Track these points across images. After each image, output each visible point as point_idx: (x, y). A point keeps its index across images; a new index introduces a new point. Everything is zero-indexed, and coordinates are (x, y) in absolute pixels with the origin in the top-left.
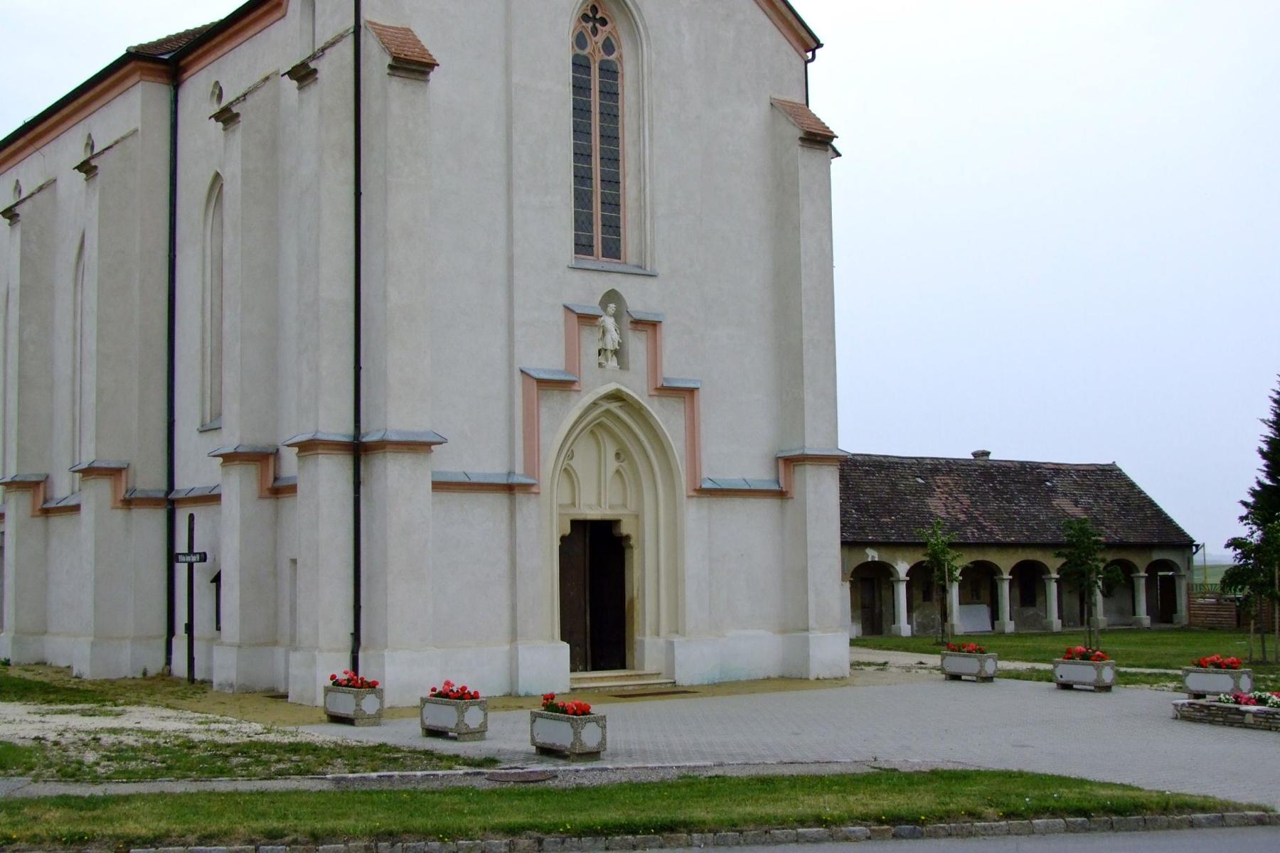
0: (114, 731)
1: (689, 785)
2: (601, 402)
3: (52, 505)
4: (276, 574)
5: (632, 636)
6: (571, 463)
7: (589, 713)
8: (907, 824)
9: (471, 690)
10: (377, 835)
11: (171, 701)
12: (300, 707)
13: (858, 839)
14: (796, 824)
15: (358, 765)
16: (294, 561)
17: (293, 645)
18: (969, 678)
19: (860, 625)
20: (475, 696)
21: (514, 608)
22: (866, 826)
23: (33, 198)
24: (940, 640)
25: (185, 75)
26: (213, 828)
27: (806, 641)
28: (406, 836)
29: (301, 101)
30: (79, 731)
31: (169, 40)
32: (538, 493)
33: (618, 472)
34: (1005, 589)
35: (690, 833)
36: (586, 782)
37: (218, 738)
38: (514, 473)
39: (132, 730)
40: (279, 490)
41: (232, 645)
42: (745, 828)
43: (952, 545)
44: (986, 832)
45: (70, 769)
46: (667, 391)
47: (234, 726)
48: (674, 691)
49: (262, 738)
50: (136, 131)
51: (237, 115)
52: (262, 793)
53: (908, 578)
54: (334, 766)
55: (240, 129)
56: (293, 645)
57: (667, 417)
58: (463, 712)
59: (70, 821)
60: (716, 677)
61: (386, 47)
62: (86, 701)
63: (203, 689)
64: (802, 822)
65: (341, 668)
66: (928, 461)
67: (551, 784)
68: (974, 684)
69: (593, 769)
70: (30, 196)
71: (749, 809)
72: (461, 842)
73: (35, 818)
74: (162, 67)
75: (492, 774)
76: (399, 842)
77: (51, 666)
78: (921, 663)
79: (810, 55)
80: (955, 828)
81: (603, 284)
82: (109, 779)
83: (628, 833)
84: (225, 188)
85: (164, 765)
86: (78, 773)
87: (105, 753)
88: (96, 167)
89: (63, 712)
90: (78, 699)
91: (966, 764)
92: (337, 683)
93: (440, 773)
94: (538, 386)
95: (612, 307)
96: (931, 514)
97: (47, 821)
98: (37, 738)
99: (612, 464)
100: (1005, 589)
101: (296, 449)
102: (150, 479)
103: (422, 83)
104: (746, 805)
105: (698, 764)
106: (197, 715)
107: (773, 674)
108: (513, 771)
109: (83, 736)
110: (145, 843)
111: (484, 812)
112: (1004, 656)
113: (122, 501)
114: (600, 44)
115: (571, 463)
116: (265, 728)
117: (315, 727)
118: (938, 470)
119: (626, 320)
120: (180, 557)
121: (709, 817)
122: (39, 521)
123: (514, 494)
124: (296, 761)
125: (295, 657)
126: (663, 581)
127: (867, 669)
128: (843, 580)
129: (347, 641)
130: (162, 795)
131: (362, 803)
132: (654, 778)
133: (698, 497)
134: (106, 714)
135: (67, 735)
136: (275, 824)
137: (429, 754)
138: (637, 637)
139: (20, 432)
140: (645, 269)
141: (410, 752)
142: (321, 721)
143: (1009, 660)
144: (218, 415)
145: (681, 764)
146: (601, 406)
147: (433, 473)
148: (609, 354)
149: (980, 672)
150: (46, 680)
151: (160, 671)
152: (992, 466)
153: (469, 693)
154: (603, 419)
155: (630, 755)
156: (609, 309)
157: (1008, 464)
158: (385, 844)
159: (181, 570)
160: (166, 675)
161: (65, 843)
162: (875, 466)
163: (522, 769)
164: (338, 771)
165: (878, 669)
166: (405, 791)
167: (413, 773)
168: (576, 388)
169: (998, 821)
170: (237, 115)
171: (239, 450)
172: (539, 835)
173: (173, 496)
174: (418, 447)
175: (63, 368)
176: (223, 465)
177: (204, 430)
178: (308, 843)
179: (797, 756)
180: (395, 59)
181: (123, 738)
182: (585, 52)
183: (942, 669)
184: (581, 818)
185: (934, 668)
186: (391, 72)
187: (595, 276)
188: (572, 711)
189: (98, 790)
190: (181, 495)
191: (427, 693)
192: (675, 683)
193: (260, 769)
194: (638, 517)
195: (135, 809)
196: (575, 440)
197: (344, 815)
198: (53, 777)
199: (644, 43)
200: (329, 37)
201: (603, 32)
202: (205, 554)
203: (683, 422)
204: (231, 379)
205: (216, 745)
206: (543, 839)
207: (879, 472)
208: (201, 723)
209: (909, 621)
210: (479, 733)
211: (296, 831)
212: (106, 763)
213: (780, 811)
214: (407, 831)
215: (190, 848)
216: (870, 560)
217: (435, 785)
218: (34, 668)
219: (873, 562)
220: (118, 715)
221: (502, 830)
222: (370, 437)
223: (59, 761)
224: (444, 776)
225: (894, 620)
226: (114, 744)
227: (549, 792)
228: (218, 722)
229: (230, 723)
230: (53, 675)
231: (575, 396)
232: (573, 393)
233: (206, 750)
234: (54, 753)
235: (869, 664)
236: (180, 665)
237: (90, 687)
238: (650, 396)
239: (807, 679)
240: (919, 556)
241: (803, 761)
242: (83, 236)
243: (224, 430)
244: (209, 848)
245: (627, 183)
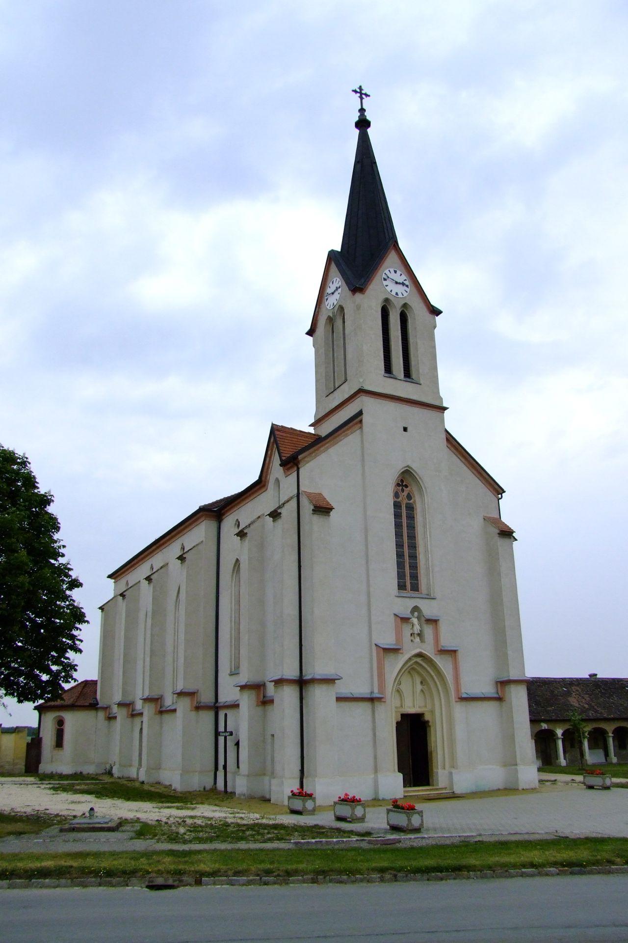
0: (192, 817)
1: (466, 846)
2: (413, 658)
3: (164, 709)
4: (264, 741)
5: (432, 770)
6: (400, 687)
7: (415, 809)
8: (577, 867)
9: (357, 797)
10: (318, 872)
11: (217, 802)
12: (277, 806)
13: (553, 875)
14: (521, 867)
15: (305, 835)
16: (273, 736)
17: (273, 775)
18: (598, 787)
19: (541, 761)
20: (360, 801)
21: (375, 758)
22: (556, 868)
23: (158, 571)
24: (581, 767)
25: (224, 517)
26: (240, 868)
27: (516, 771)
28: (331, 873)
29: (274, 526)
30: (176, 817)
31: (217, 502)
32: (385, 702)
33: (422, 691)
34: (611, 741)
35: (468, 871)
36: (415, 844)
37: (239, 821)
38: (374, 692)
39: (200, 817)
40: (266, 702)
41: (244, 776)
42: (496, 869)
43: (583, 720)
44: (618, 872)
45: (173, 836)
46: (443, 652)
47: (246, 815)
48: (453, 796)
49: (260, 821)
50: (202, 542)
51: (246, 533)
52: (262, 850)
53: (562, 737)
54: (295, 836)
55: (247, 539)
56: (273, 775)
57: (444, 664)
58: (354, 809)
59: (174, 863)
60: (473, 788)
61: (311, 501)
62: (178, 802)
63: (231, 796)
64: (524, 866)
65: (296, 788)
66: (568, 680)
67: (398, 845)
68: (601, 791)
69: (418, 838)
70: (157, 571)
71: (497, 859)
72: (357, 876)
73: (159, 861)
75: (369, 840)
76: (327, 876)
77: (162, 784)
78: (573, 780)
79: (500, 496)
80: (602, 869)
81: (411, 603)
82: (190, 842)
83: (438, 872)
84: (241, 565)
85: (215, 835)
86: (177, 838)
87: (188, 828)
88: (185, 558)
89: (168, 807)
90: (175, 801)
91: (602, 834)
92: (294, 794)
93: (344, 839)
94: (383, 652)
95: (416, 614)
96: (571, 705)
97: (164, 863)
98: (157, 820)
99: (419, 687)
100: (611, 741)
101: (274, 683)
102: (207, 697)
103: (327, 517)
104: (495, 857)
105: (469, 834)
106: (229, 809)
107: (501, 787)
108: (380, 839)
109: (178, 819)
110: (209, 875)
111: (368, 861)
112: (615, 776)
113: (195, 707)
114: (405, 496)
115: (400, 687)
116: (261, 816)
117: (284, 816)
118: (573, 683)
119: (423, 619)
120: (221, 734)
121: (477, 863)
122: (158, 717)
123: (374, 702)
124: (276, 833)
125: (274, 781)
126: (446, 743)
127: (547, 783)
128: (532, 739)
129: (298, 774)
130: (215, 850)
131: (310, 855)
132: (448, 842)
133: (460, 701)
134: (188, 809)
135: (171, 819)
136: (268, 866)
137: (339, 830)
138: (435, 770)
139: (150, 676)
140: (430, 596)
141: (329, 829)
142: (287, 813)
143: (617, 777)
144: (238, 667)
145: (461, 835)
146: (413, 660)
147: (336, 693)
148: (416, 636)
149: (603, 785)
150: (161, 791)
151: (211, 787)
152: (599, 681)
153: (356, 799)
154: (414, 666)
155: (435, 830)
156: (415, 615)
157: (606, 679)
158: (321, 877)
159: (221, 739)
160: (214, 789)
161: (173, 874)
162: (542, 683)
163: (384, 837)
164: (296, 838)
165: (552, 784)
166: (329, 849)
167: (332, 840)
168: (401, 651)
169: (623, 865)
170: (246, 533)
171: (248, 684)
172: (395, 873)
173: (217, 705)
174: (329, 681)
175: (169, 648)
176: (240, 690)
177: (231, 674)
178: (284, 876)
179: (517, 830)
180: (315, 507)
181: (196, 821)
182: (399, 500)
183: (584, 783)
184: (415, 864)
185: (580, 782)
186: (313, 512)
187: (408, 600)
188: (406, 808)
189: (186, 847)
190: (221, 704)
191: (337, 799)
192: (453, 792)
193: (259, 837)
194: (432, 712)
195: (203, 857)
197: (301, 862)
198: (165, 840)
199: (425, 494)
200: (286, 498)
201: (407, 491)
202: (232, 732)
203: (451, 666)
204: (244, 652)
205: (238, 825)
206: (397, 875)
208: (231, 814)
209: (565, 758)
210: (362, 819)
211: (279, 870)
212: (189, 833)
213: (512, 861)
214: (332, 871)
215: (230, 878)
216: (543, 728)
217: (343, 846)
218: (156, 785)
219: (545, 730)
220: (193, 809)
221: (377, 870)
222: (307, 677)
223: (168, 832)
224: (346, 841)
225: (557, 757)
226: (192, 824)
227: (398, 850)
228: (238, 813)
229: (245, 814)
230: (164, 789)
231: (401, 655)
232: (399, 654)
233: (234, 827)
234: (166, 828)
235: (547, 781)
236: (220, 785)
237: (180, 795)
238: (435, 654)
239: (518, 789)
240: (567, 726)
241: (521, 832)
242: (179, 587)
243: (241, 675)
244: (238, 878)
245: (420, 557)
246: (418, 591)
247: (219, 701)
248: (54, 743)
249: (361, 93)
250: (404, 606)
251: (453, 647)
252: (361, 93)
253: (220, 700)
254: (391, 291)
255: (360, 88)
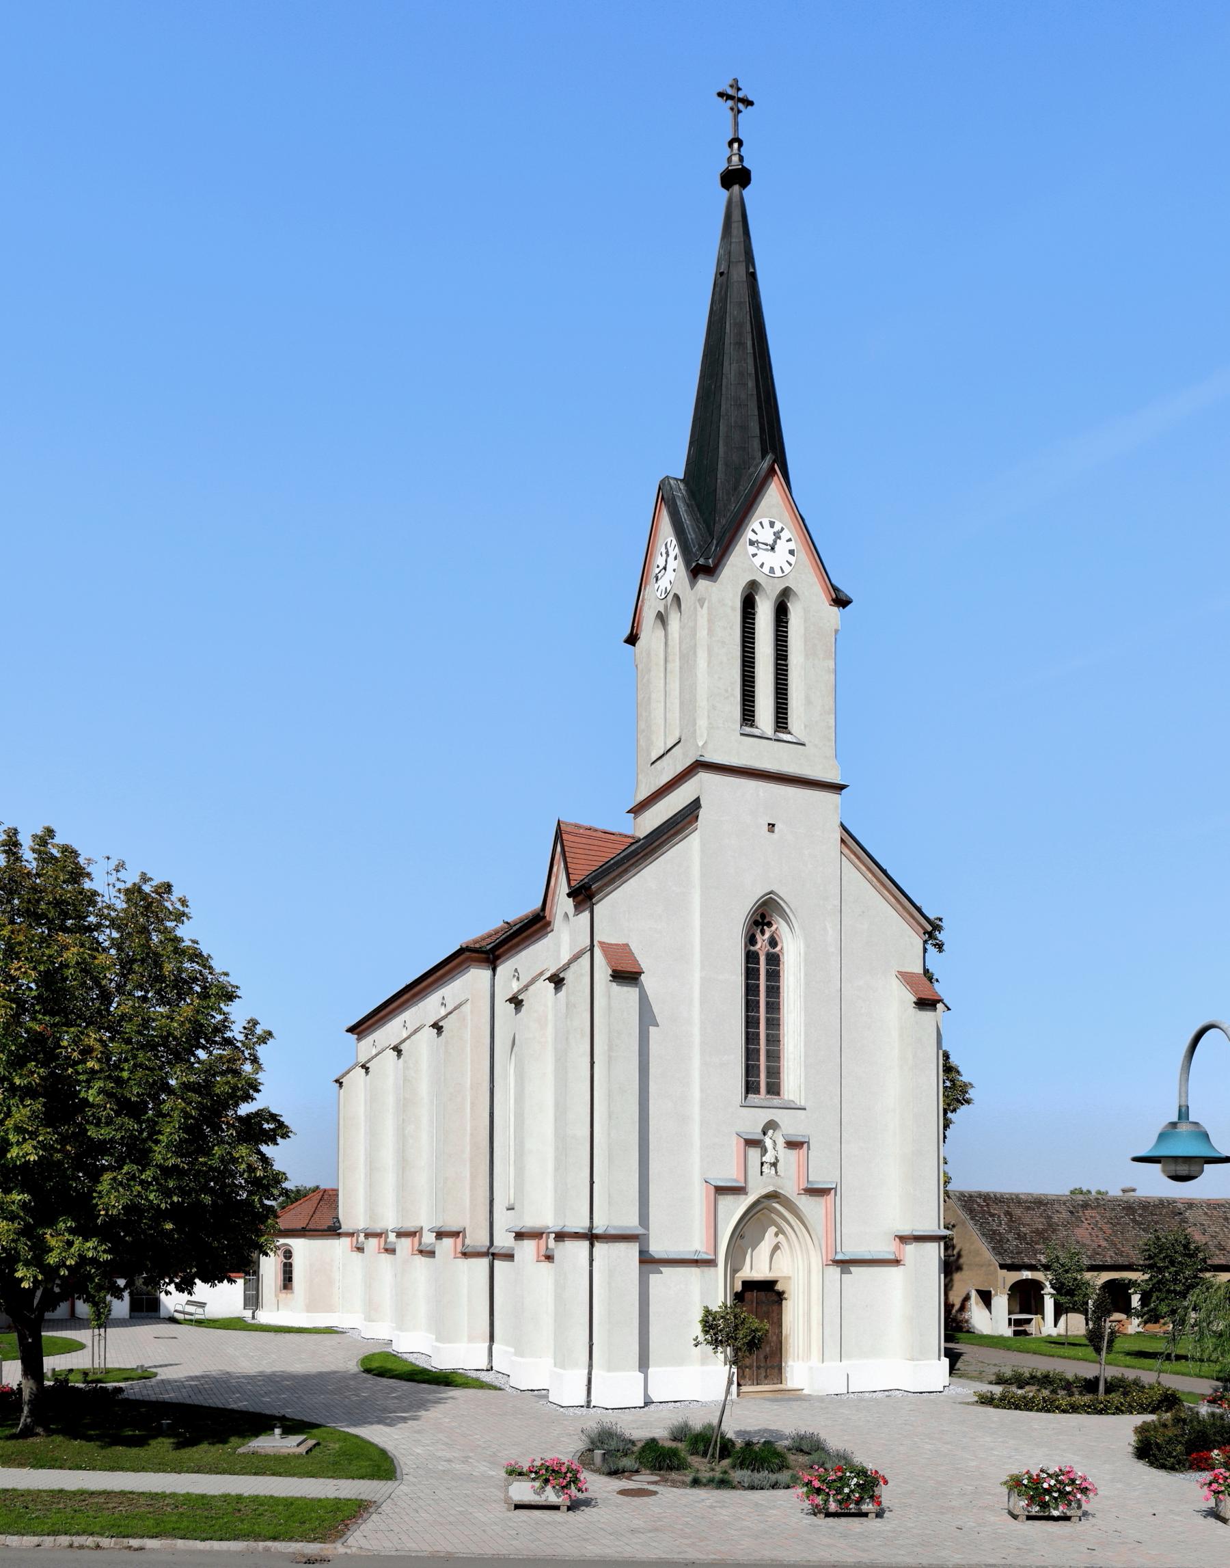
2: (763, 1200)
61: (609, 962)
74: (484, 956)
162: (1034, 1203)
170: (522, 1001)
196: (749, 1220)
207: (1039, 1208)
246: (778, 1094)
247: (495, 1244)
248: (280, 1282)
249: (737, 100)
250: (753, 1121)
251: (824, 1182)
252: (737, 100)
253: (496, 1243)
254: (762, 566)
255: (736, 86)
